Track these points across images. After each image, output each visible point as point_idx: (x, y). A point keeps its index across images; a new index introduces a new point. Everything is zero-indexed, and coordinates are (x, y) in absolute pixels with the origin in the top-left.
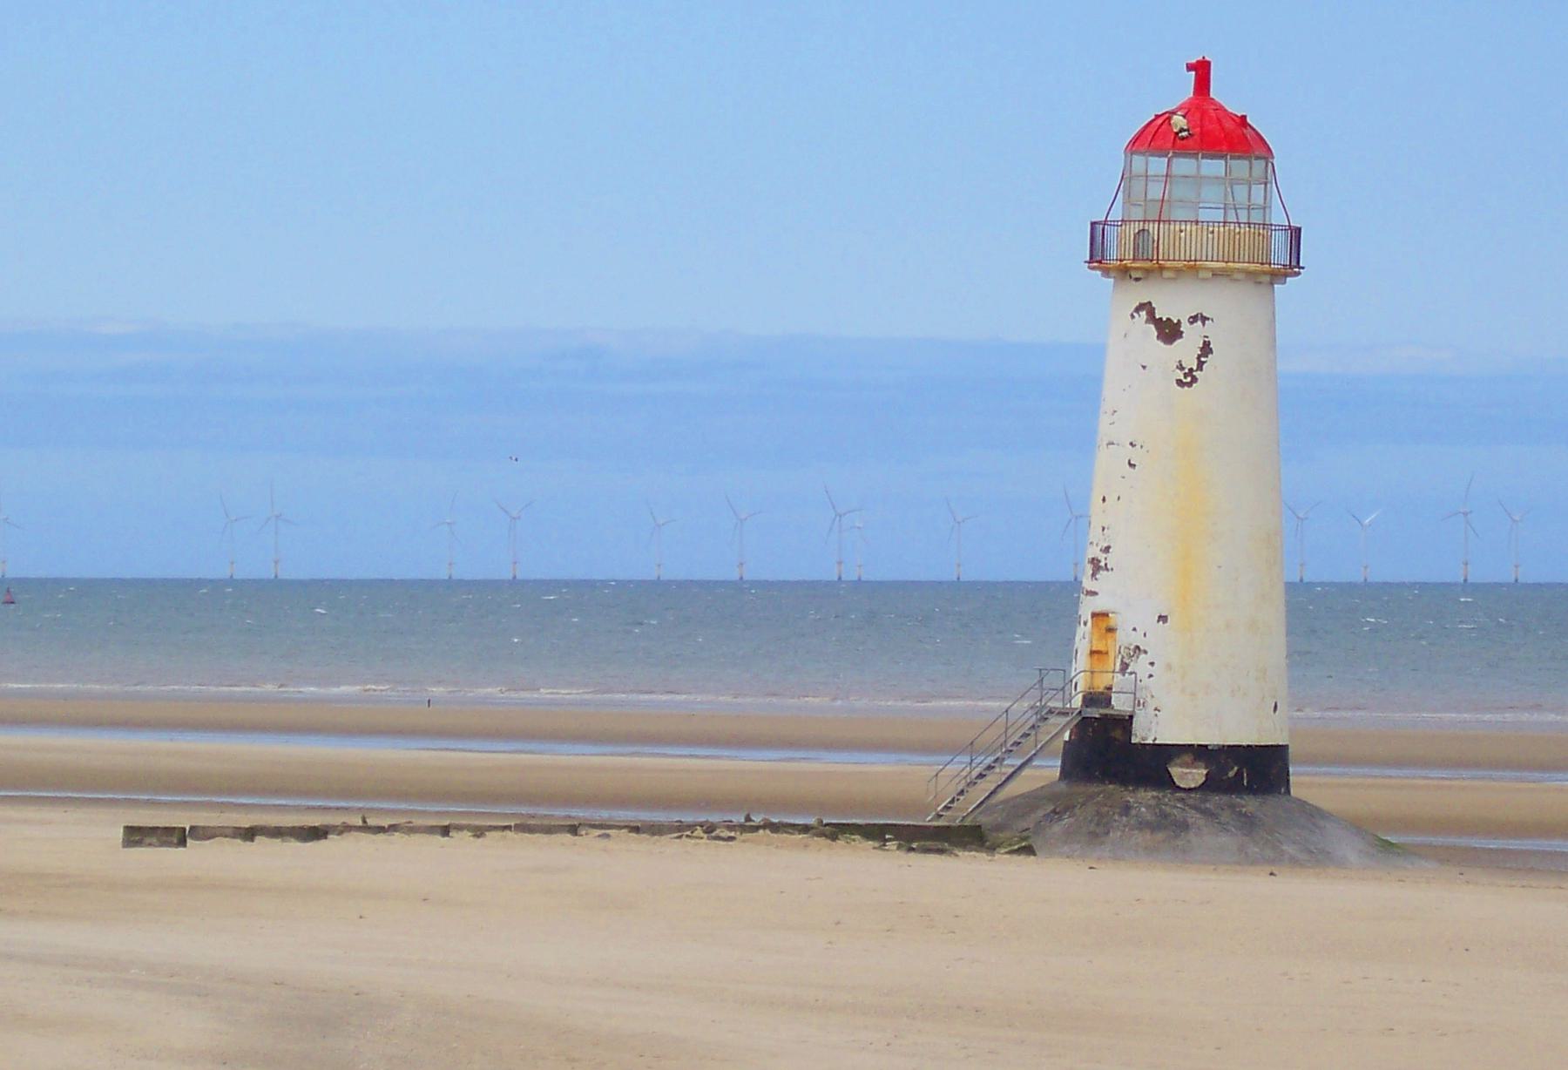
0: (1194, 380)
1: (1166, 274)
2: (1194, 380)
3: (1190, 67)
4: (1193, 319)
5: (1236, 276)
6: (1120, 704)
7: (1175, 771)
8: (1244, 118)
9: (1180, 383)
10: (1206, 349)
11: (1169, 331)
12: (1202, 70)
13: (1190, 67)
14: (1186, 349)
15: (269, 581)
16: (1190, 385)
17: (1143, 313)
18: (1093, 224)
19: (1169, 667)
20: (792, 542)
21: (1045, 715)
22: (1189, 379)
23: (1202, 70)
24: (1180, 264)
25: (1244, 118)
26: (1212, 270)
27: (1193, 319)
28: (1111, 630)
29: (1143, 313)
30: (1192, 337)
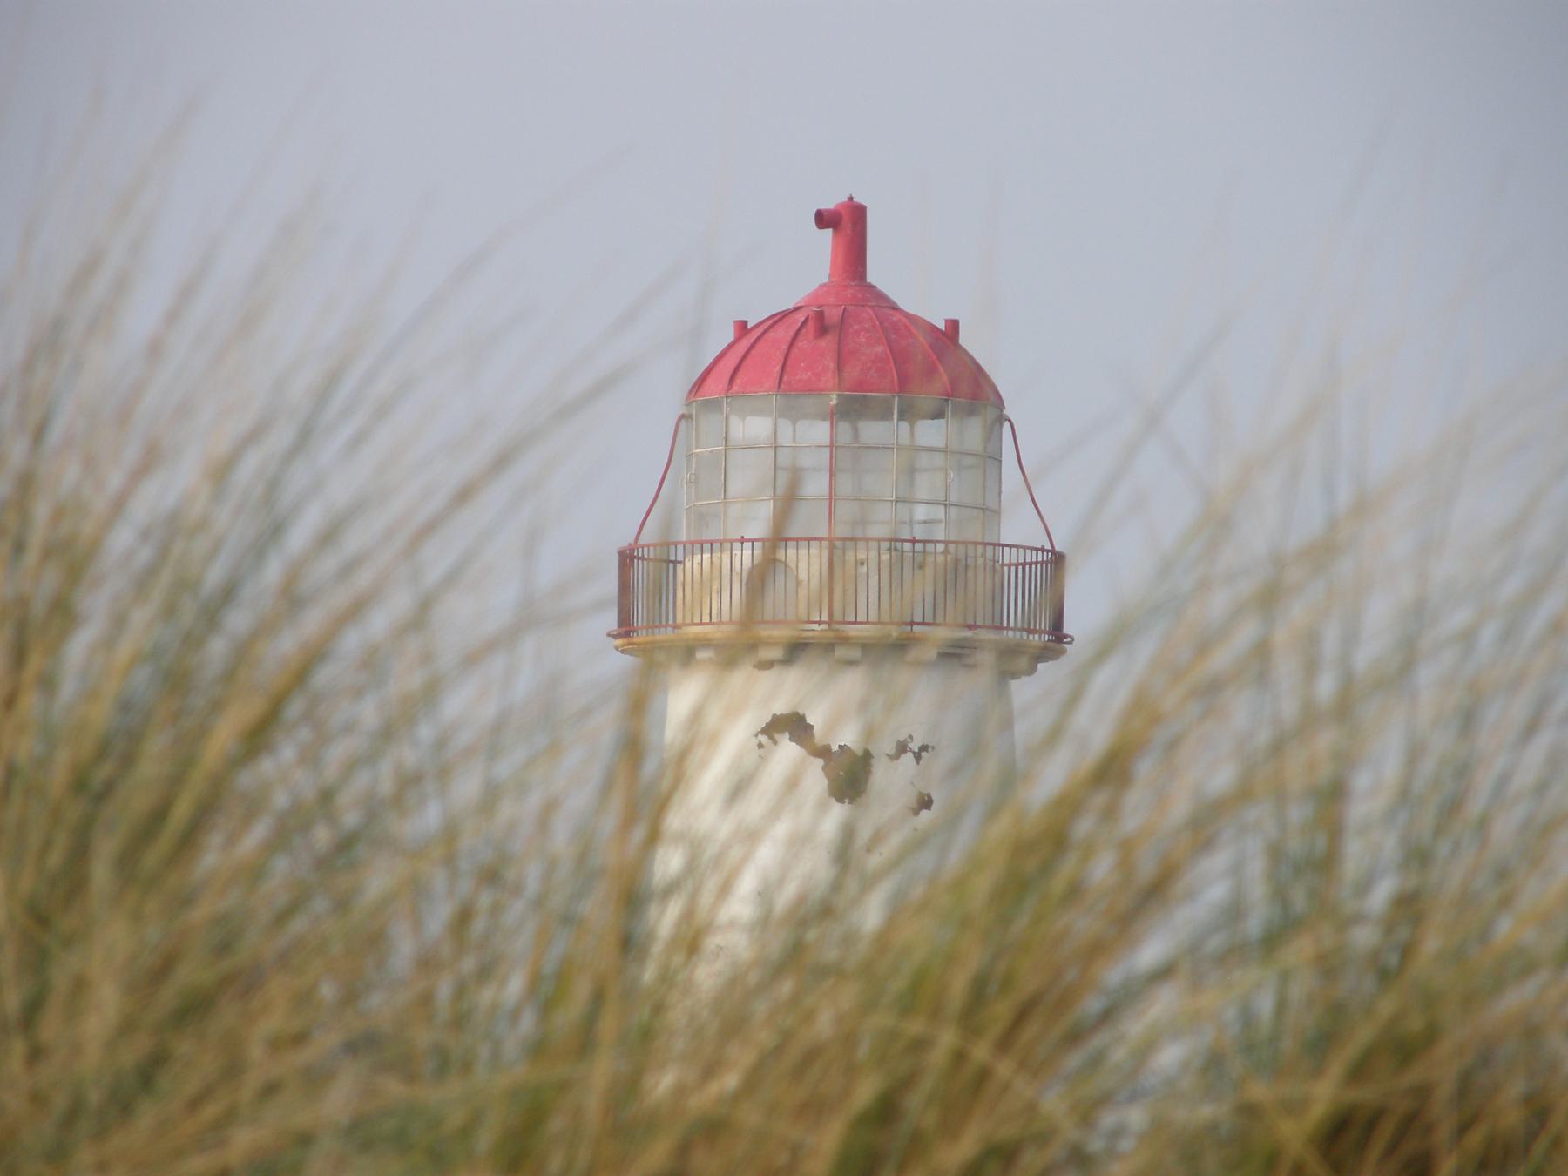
1: (840, 652)
5: (702, 655)
25: (742, 328)
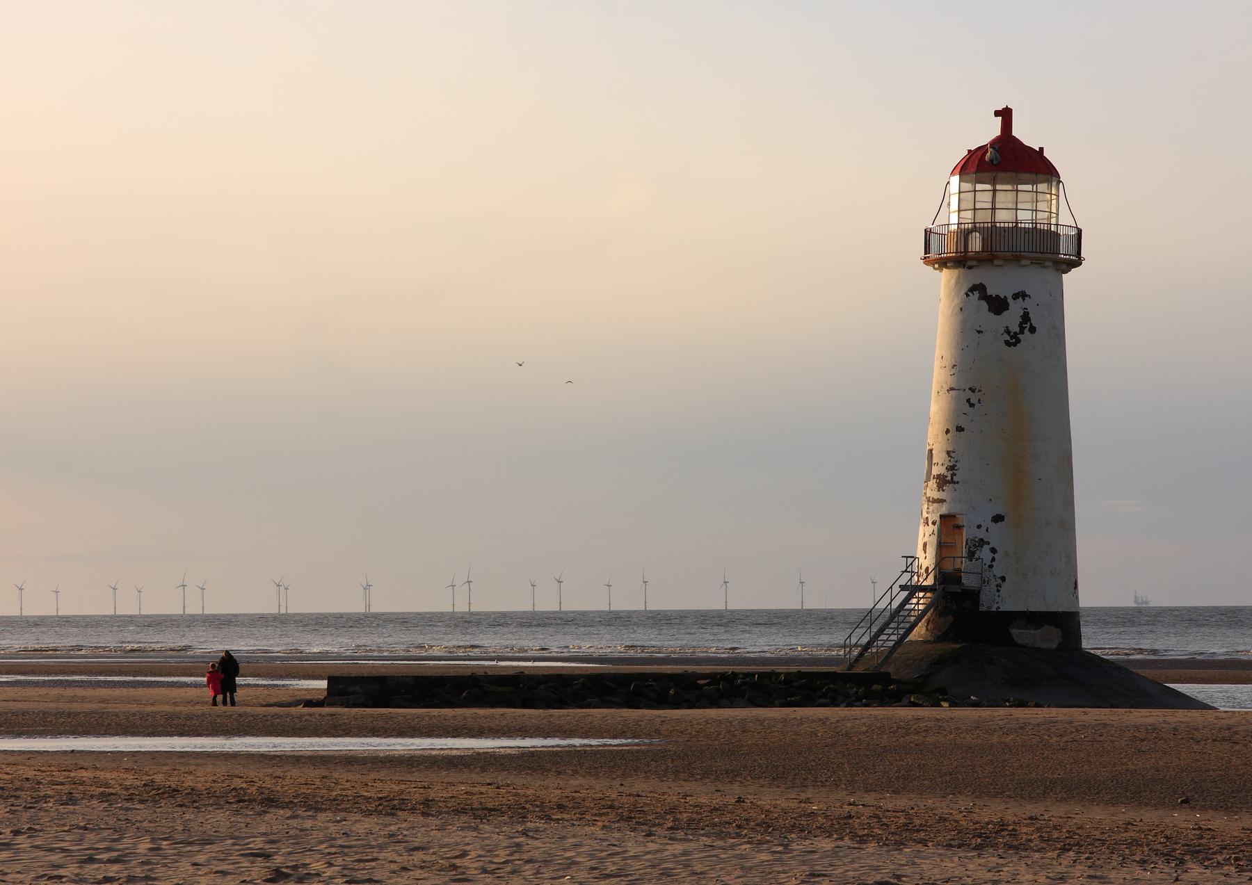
0: (1018, 341)
1: (996, 262)
2: (1018, 341)
3: (997, 113)
4: (1016, 296)
6: (969, 581)
7: (1014, 632)
8: (969, 151)
9: (1007, 343)
10: (1026, 317)
11: (998, 305)
12: (1005, 115)
13: (997, 113)
14: (1011, 319)
15: (111, 617)
16: (1015, 345)
17: (977, 294)
18: (928, 233)
19: (1007, 553)
20: (441, 651)
21: (912, 590)
22: (1013, 340)
23: (1005, 115)
24: (1009, 254)
25: (969, 151)
26: (1031, 259)
27: (1016, 296)
28: (959, 527)
29: (977, 294)
30: (1016, 308)
